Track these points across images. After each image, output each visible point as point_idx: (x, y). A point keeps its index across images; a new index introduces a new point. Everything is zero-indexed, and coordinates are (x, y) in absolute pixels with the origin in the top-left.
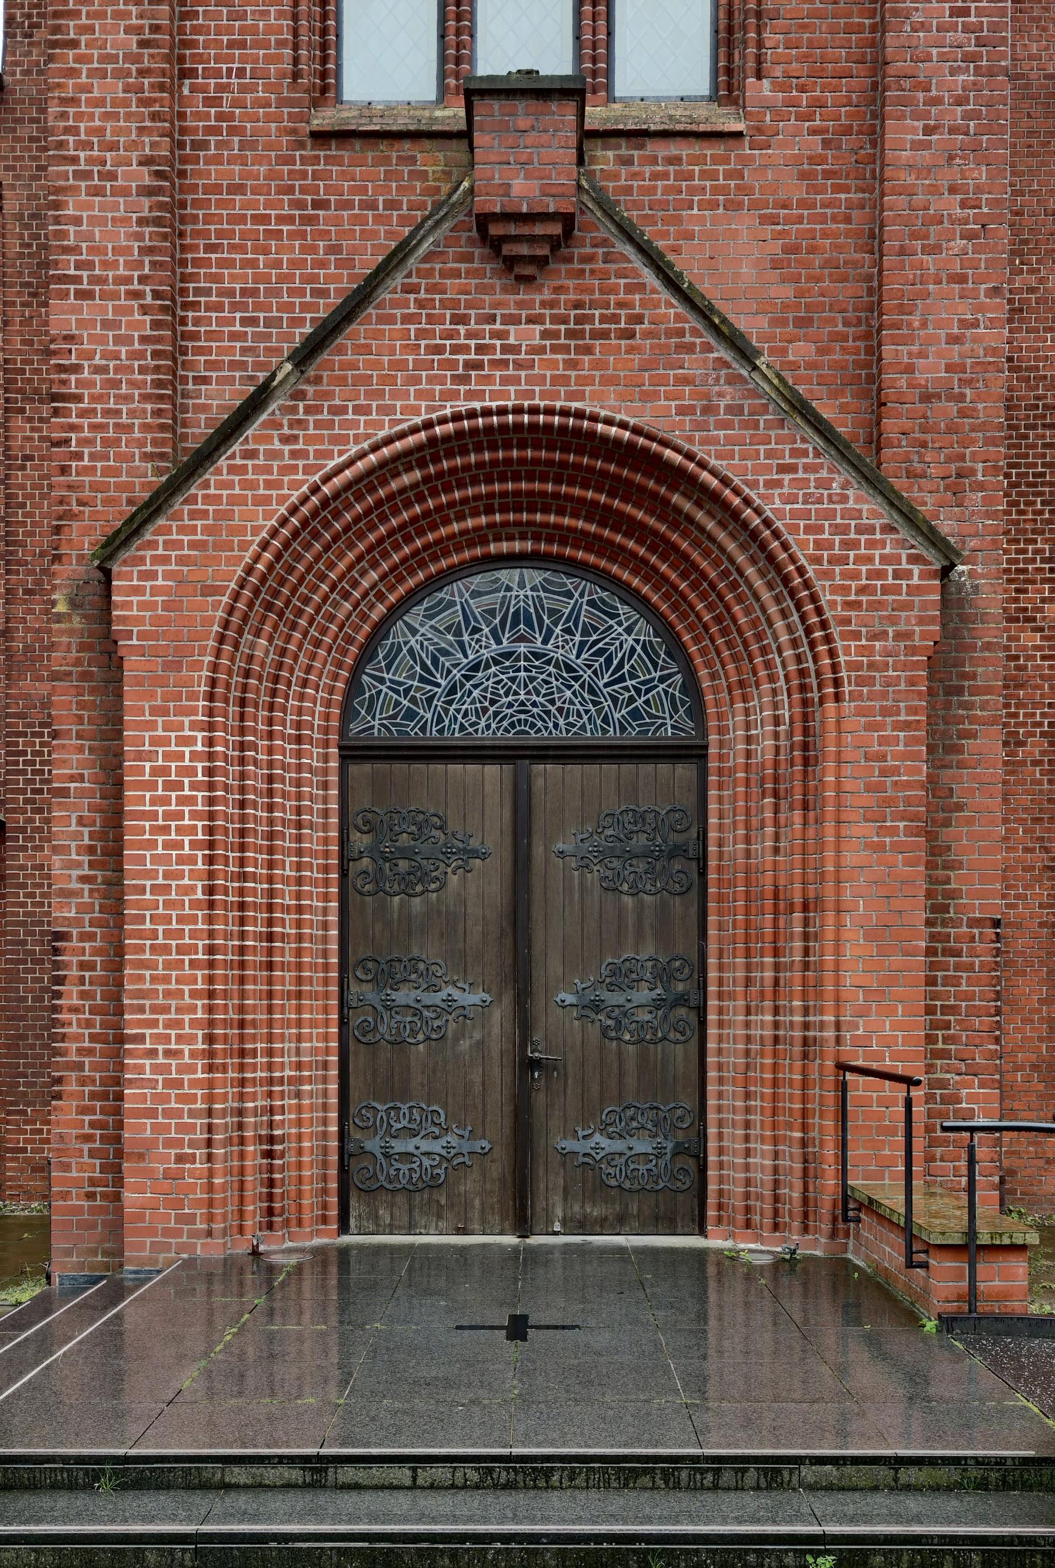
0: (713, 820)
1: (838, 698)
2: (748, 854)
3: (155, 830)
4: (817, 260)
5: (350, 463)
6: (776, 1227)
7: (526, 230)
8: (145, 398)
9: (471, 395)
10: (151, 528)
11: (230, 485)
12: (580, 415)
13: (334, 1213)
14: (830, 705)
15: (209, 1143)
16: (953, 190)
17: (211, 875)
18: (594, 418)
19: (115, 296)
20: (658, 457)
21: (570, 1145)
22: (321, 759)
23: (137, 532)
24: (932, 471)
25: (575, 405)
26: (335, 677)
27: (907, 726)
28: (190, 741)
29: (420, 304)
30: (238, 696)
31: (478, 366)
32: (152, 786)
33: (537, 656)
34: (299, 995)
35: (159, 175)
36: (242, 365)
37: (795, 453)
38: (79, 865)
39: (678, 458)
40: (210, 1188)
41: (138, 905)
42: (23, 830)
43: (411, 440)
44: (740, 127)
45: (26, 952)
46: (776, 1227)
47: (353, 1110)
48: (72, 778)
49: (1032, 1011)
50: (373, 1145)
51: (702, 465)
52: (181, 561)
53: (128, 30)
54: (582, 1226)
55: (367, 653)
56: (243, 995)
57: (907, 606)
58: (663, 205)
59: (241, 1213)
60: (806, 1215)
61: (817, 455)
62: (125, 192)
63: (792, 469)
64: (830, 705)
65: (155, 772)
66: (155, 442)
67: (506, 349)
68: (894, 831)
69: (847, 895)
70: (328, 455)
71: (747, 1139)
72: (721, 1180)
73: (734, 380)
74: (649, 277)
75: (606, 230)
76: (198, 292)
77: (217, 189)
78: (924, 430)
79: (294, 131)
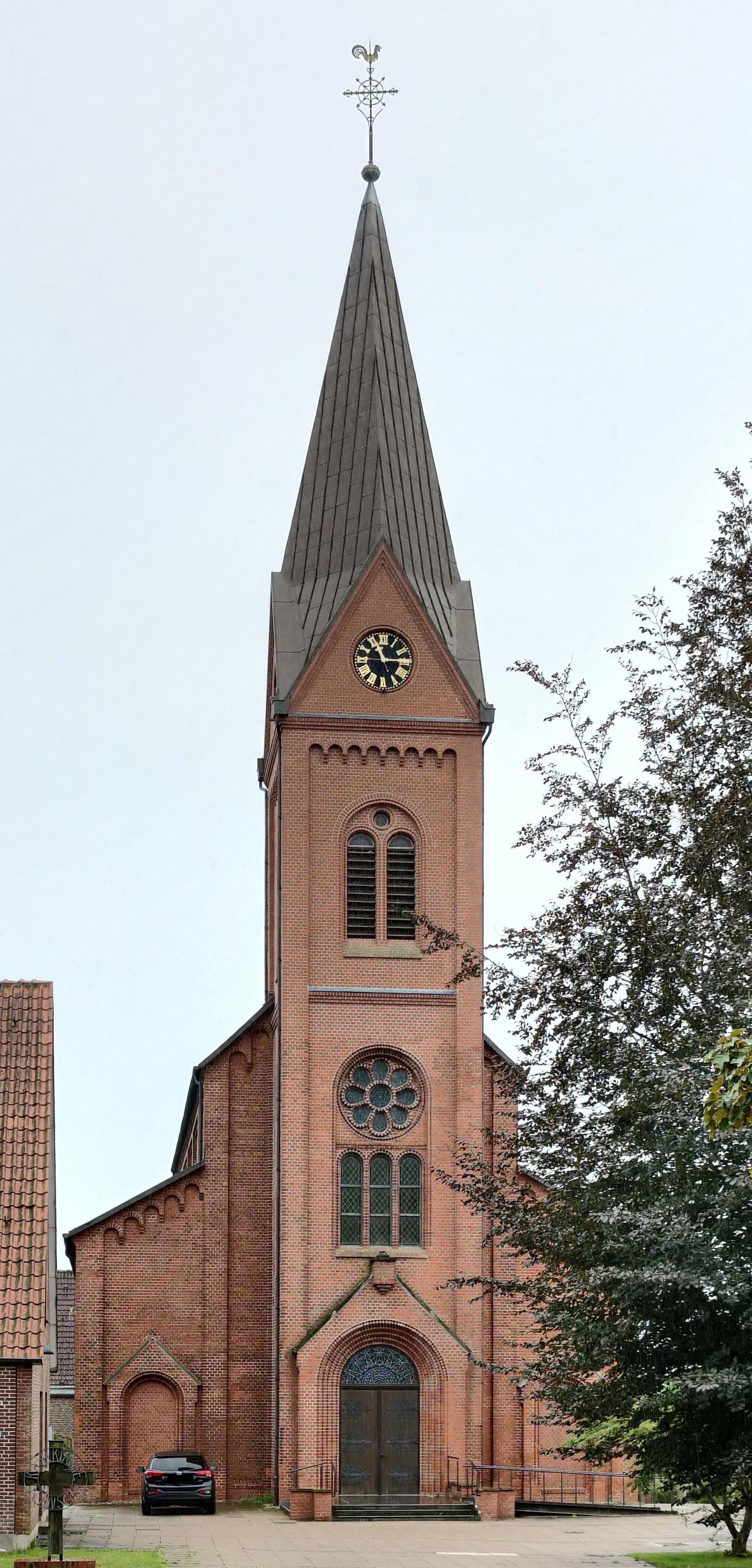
21: (390, 1474)
30: (323, 1378)
44: (426, 1257)
50: (346, 1474)
74: (409, 1294)
75: (400, 1284)
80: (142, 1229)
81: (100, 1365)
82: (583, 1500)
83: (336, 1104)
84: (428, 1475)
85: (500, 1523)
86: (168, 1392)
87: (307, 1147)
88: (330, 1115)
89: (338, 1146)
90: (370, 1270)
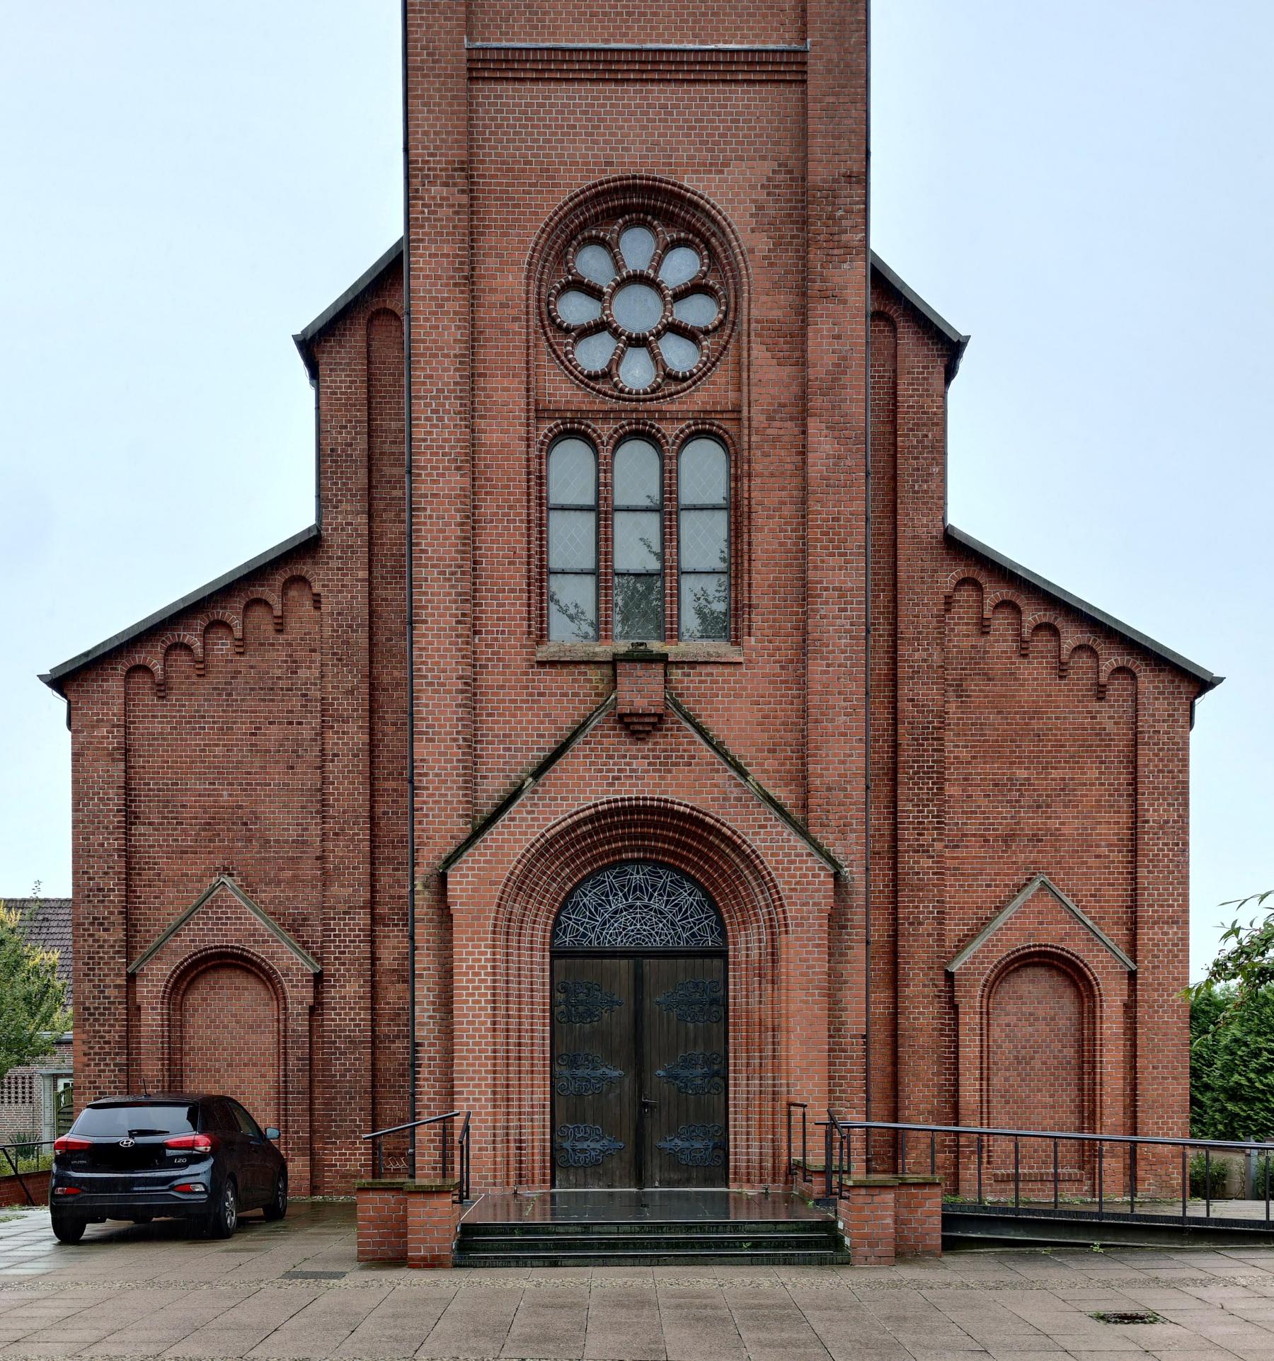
0: (731, 987)
1: (787, 932)
2: (747, 1003)
3: (468, 995)
4: (778, 721)
5: (559, 823)
6: (761, 1181)
7: (641, 720)
8: (459, 788)
9: (616, 792)
10: (466, 854)
11: (502, 834)
12: (666, 801)
13: (548, 1178)
14: (783, 936)
15: (494, 1142)
16: (840, 693)
17: (494, 1016)
18: (673, 803)
19: (444, 740)
20: (703, 821)
21: (663, 1144)
22: (541, 958)
23: (459, 856)
24: (832, 823)
25: (664, 797)
26: (548, 918)
27: (818, 946)
28: (485, 953)
29: (591, 750)
30: (506, 929)
31: (618, 778)
32: (467, 974)
33: (646, 907)
34: (532, 1072)
35: (466, 683)
36: (503, 770)
37: (766, 819)
38: (428, 1010)
39: (712, 822)
40: (495, 1163)
41: (461, 1030)
42: (333, 975)
43: (587, 813)
44: (741, 659)
45: (336, 1048)
46: (761, 1181)
47: (557, 1128)
48: (424, 969)
49: (929, 1080)
50: (567, 1145)
51: (723, 824)
52: (479, 869)
53: (451, 615)
54: (669, 1184)
55: (563, 906)
56: (508, 1072)
57: (818, 890)
58: (705, 695)
59: (508, 1175)
60: (774, 1174)
61: (776, 820)
62: (449, 692)
63: (765, 826)
64: (783, 936)
65: (468, 968)
66: (464, 809)
67: (632, 771)
68: (813, 995)
69: (791, 1025)
70: (548, 819)
71: (748, 1140)
72: (736, 1160)
73: (738, 785)
74: (698, 738)
76: (482, 735)
77: (492, 687)
78: (828, 804)
79: (529, 660)
80: (203, 667)
81: (121, 935)
82: (1074, 1198)
83: (534, 321)
84: (747, 1145)
85: (906, 1273)
86: (260, 987)
87: (471, 413)
88: (519, 341)
89: (541, 413)
90: (614, 681)
